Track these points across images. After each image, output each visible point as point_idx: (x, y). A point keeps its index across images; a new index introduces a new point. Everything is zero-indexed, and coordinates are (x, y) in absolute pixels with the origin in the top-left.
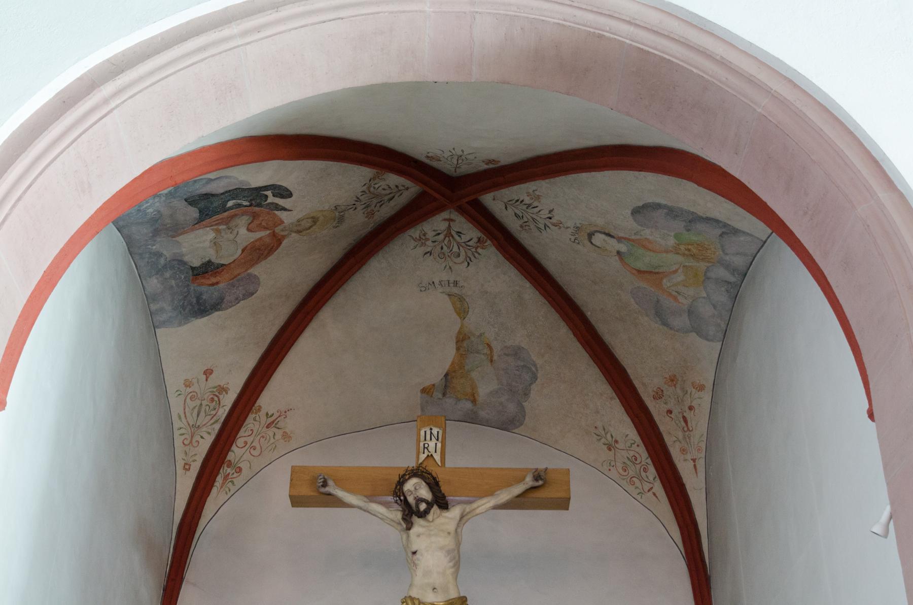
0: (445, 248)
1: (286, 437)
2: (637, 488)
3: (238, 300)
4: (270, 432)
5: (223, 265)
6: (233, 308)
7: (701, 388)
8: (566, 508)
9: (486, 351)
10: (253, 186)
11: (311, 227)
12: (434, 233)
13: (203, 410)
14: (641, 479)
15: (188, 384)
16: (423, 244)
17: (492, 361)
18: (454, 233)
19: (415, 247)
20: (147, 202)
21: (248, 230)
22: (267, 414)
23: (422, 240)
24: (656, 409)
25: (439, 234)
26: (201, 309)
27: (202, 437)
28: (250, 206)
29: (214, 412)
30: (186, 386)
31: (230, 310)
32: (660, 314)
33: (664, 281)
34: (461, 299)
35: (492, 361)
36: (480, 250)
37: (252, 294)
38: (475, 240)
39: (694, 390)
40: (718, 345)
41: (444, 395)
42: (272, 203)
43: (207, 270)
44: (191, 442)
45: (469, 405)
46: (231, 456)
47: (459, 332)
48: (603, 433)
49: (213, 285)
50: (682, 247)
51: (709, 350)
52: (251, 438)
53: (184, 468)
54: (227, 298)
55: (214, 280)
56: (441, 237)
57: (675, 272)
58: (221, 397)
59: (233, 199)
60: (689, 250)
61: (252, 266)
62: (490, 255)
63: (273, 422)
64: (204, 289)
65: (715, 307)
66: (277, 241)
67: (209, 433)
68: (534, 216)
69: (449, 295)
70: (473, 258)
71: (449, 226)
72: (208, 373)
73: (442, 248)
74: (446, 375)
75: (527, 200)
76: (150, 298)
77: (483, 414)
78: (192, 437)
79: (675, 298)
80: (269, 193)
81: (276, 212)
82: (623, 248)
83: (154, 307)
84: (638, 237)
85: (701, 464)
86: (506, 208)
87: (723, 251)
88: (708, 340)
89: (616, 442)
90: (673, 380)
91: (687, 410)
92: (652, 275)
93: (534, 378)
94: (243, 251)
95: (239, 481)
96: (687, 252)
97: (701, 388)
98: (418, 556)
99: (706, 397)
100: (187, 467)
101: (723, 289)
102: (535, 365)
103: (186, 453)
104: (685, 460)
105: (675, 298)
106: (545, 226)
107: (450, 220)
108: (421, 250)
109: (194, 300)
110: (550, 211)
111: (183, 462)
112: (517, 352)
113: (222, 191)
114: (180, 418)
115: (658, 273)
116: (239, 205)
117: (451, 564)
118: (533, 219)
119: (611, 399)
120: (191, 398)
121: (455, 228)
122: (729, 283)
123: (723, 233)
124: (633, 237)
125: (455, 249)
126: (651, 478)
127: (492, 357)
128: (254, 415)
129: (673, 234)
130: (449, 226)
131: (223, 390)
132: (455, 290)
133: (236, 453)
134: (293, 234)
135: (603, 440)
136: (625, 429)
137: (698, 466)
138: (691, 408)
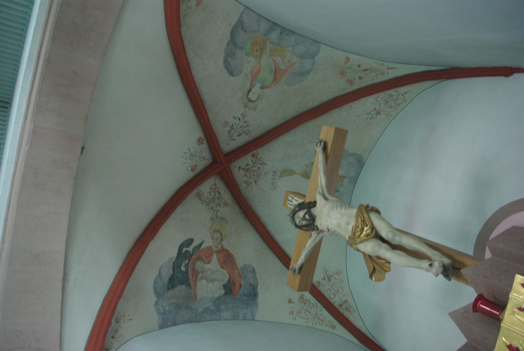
0: (254, 173)
1: (338, 273)
3: (255, 277)
4: (333, 280)
5: (229, 280)
7: (348, 59)
8: (346, 132)
10: (176, 256)
11: (221, 233)
12: (245, 177)
14: (397, 99)
15: (292, 313)
16: (251, 183)
18: (247, 168)
19: (252, 187)
20: (159, 308)
21: (209, 263)
23: (248, 183)
24: (358, 85)
25: (246, 175)
26: (253, 295)
27: (322, 314)
28: (190, 260)
29: (311, 305)
31: (259, 282)
32: (303, 74)
36: (259, 157)
37: (254, 270)
38: (253, 158)
39: (349, 63)
42: (193, 249)
43: (229, 288)
45: (346, 180)
46: (336, 305)
47: (303, 176)
49: (240, 286)
50: (255, 54)
53: (333, 328)
54: (252, 281)
55: (237, 286)
56: (248, 174)
57: (274, 61)
58: (305, 298)
59: (180, 267)
60: (257, 51)
61: (236, 266)
62: (262, 152)
63: (328, 277)
64: (241, 292)
65: (298, 44)
66: (223, 250)
67: (321, 310)
68: (239, 127)
69: (281, 177)
71: (243, 169)
72: (290, 301)
73: (254, 175)
76: (235, 318)
78: (320, 319)
79: (292, 64)
80: (184, 249)
81: (491, 238)
82: (258, 85)
84: (249, 75)
85: (393, 65)
86: (234, 140)
89: (375, 109)
90: (343, 73)
92: (277, 74)
94: (223, 268)
95: (351, 303)
96: (259, 52)
97: (348, 59)
98: (329, 228)
99: (352, 57)
100: (333, 327)
104: (388, 73)
105: (292, 64)
106: (245, 122)
107: (239, 168)
108: (253, 185)
109: (246, 298)
111: (330, 328)
113: (171, 272)
114: (307, 322)
115: (275, 71)
117: (339, 208)
118: (240, 127)
119: (351, 107)
121: (244, 166)
122: (281, 33)
123: (242, 29)
124: (250, 78)
125: (256, 169)
126: (396, 94)
128: (321, 286)
129: (246, 57)
130: (243, 169)
132: (279, 173)
133: (336, 301)
134: (223, 243)
135: (374, 116)
136: (368, 103)
137: (392, 67)
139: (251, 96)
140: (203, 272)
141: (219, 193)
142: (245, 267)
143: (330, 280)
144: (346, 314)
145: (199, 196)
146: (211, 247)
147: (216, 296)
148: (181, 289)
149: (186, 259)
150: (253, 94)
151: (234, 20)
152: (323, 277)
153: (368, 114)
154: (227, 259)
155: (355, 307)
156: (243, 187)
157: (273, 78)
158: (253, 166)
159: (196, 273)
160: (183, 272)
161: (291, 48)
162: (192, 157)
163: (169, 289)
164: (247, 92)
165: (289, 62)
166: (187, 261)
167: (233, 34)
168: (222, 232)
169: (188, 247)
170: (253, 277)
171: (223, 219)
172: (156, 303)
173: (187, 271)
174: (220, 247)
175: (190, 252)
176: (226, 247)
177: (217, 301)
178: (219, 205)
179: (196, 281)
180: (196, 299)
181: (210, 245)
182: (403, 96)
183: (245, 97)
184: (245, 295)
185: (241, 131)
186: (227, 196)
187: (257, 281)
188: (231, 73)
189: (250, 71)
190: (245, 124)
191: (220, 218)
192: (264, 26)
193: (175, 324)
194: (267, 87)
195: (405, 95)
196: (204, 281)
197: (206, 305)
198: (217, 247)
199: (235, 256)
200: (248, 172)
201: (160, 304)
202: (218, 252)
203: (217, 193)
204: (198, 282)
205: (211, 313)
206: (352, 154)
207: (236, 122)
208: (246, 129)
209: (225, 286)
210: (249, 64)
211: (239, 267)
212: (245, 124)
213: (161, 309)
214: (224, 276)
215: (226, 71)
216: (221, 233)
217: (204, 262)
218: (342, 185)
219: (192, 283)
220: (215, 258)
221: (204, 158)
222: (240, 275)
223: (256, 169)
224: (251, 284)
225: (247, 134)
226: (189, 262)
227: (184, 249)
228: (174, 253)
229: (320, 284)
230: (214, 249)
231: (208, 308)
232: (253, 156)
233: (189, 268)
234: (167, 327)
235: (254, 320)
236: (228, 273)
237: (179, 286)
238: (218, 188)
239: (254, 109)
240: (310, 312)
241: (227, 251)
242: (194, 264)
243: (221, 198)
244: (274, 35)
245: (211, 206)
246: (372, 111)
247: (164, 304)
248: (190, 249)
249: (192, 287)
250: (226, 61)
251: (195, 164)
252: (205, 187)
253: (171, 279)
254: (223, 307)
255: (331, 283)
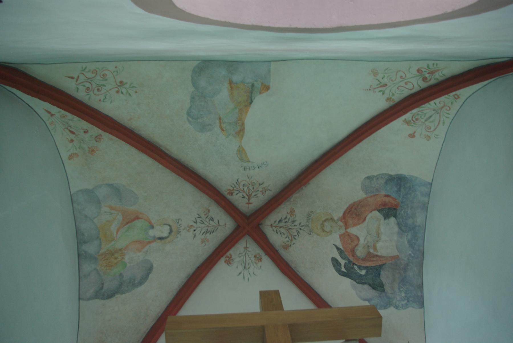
0: (251, 189)
1: (375, 73)
2: (89, 71)
3: (377, 177)
4: (385, 81)
6: (382, 173)
7: (71, 157)
9: (224, 125)
10: (350, 280)
12: (258, 195)
13: (426, 118)
15: (428, 138)
16: (264, 188)
17: (220, 119)
19: (269, 186)
20: (402, 305)
21: (358, 239)
22: (383, 94)
25: (255, 195)
26: (399, 181)
28: (354, 264)
29: (420, 113)
30: (430, 137)
32: (117, 191)
33: (121, 218)
34: (241, 159)
35: (220, 119)
36: (232, 188)
37: (368, 178)
38: (234, 194)
39: (75, 152)
40: (73, 191)
41: (253, 85)
43: (389, 211)
44: (444, 106)
47: (242, 136)
48: (130, 91)
49: (388, 196)
50: (120, 258)
51: (78, 184)
52: (400, 84)
54: (382, 181)
55: (387, 199)
56: (253, 194)
57: (118, 231)
58: (410, 119)
59: (361, 276)
60: (116, 258)
63: (381, 86)
64: (394, 195)
65: (86, 217)
68: (203, 225)
69: (249, 161)
70: (235, 184)
71: (249, 201)
72: (412, 136)
73: (253, 188)
74: (251, 102)
75: (208, 236)
76: (425, 207)
77: (223, 72)
78: (442, 108)
79: (111, 208)
80: (343, 269)
81: (342, 249)
82: (152, 233)
83: (426, 199)
84: (145, 249)
87: (97, 271)
88: (81, 190)
89: (118, 92)
90: (92, 151)
91: (73, 138)
92: (130, 219)
93: (189, 113)
94: (365, 219)
95: (423, 65)
96: (116, 255)
97: (71, 157)
99: (65, 155)
100: (457, 97)
101: (86, 235)
102: (190, 122)
103: (452, 103)
105: (111, 208)
107: (249, 203)
109: (402, 189)
110: (195, 236)
111: (457, 100)
112: (204, 128)
113: (366, 287)
114: (444, 123)
115: (128, 223)
116: (360, 268)
118: (204, 223)
120: (430, 128)
122: (85, 242)
123: (102, 288)
125: (245, 189)
126: (81, 87)
127: (220, 122)
128: (393, 97)
129: (128, 265)
130: (249, 201)
131: (408, 122)
132: (245, 164)
133: (416, 84)
138: (72, 141)
139: (165, 234)
140: (368, 246)
141: (280, 221)
142: (365, 188)
143: (386, 85)
144: (439, 76)
145: (286, 247)
146: (340, 236)
147: (396, 229)
148: (385, 277)
149: (353, 268)
150: (162, 232)
151: (98, 302)
152: (381, 93)
153: (130, 95)
154: (354, 213)
155: (430, 63)
156: (269, 194)
157: (136, 221)
158: (244, 191)
159: (370, 256)
160: (367, 272)
161: (95, 221)
162: (247, 266)
163: (384, 291)
164: (163, 241)
165: (111, 213)
166: (356, 267)
167: (111, 295)
168: (323, 219)
169: (341, 265)
170: (377, 179)
171: (309, 216)
172: (397, 307)
173: (366, 268)
174: (340, 223)
175: (345, 263)
176: (341, 214)
177: (403, 228)
178: (293, 222)
179: (377, 256)
180: (398, 256)
181: (338, 236)
182: (78, 77)
183: (169, 239)
184: (399, 190)
185: (207, 220)
186: (282, 212)
187: (383, 174)
188: (150, 269)
189: (140, 251)
190: (198, 220)
191: (308, 221)
192: (87, 267)
193: (421, 287)
194: (150, 222)
195: (76, 77)
196: (379, 245)
197: (406, 243)
198: (341, 226)
199: (352, 202)
200: (251, 195)
201: (398, 302)
202: (347, 226)
203: (280, 225)
204: (379, 254)
205: (414, 235)
206: (195, 84)
207: (199, 232)
208: (203, 216)
209: (387, 217)
210: (133, 258)
211: (364, 196)
212: (198, 220)
213: (403, 303)
214: (374, 217)
215: (151, 276)
216: (325, 221)
217: (357, 245)
218: (243, 82)
219: (380, 263)
220: (353, 231)
221: (246, 248)
222: (374, 196)
223: (245, 189)
224: (386, 183)
225: (209, 211)
226: (356, 265)
227: (343, 269)
228: (347, 282)
229: (391, 98)
230: (342, 231)
231: (409, 242)
232: (232, 194)
233: (363, 265)
234: (422, 297)
235: (431, 184)
236: (371, 212)
237: (382, 279)
238: (275, 222)
239: (178, 221)
240: (431, 117)
241: (344, 213)
242: (358, 259)
243: (286, 218)
244: (91, 248)
245: (296, 234)
246: (122, 93)
247: (398, 298)
248: (343, 262)
249: (384, 262)
250: (141, 283)
251: (253, 259)
252: (276, 239)
253: (374, 287)
254: (410, 221)
255: (389, 85)
